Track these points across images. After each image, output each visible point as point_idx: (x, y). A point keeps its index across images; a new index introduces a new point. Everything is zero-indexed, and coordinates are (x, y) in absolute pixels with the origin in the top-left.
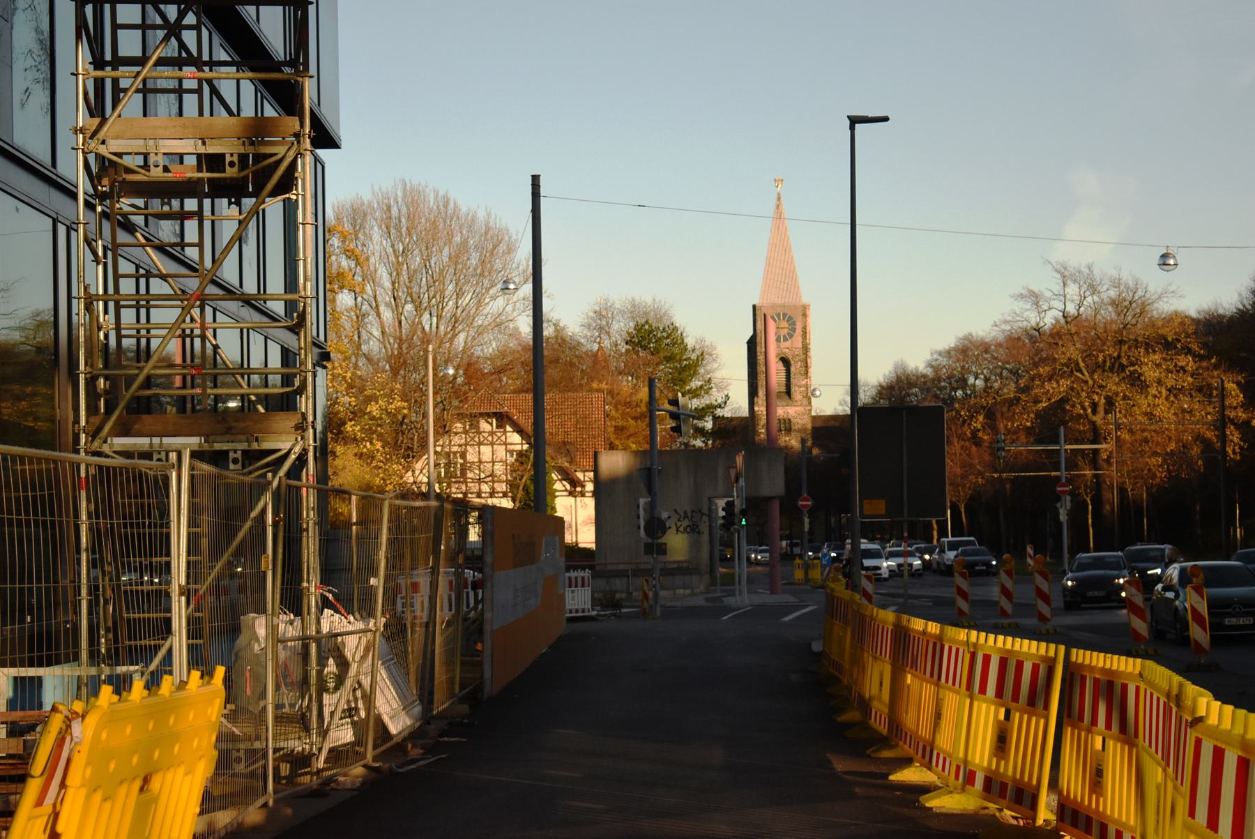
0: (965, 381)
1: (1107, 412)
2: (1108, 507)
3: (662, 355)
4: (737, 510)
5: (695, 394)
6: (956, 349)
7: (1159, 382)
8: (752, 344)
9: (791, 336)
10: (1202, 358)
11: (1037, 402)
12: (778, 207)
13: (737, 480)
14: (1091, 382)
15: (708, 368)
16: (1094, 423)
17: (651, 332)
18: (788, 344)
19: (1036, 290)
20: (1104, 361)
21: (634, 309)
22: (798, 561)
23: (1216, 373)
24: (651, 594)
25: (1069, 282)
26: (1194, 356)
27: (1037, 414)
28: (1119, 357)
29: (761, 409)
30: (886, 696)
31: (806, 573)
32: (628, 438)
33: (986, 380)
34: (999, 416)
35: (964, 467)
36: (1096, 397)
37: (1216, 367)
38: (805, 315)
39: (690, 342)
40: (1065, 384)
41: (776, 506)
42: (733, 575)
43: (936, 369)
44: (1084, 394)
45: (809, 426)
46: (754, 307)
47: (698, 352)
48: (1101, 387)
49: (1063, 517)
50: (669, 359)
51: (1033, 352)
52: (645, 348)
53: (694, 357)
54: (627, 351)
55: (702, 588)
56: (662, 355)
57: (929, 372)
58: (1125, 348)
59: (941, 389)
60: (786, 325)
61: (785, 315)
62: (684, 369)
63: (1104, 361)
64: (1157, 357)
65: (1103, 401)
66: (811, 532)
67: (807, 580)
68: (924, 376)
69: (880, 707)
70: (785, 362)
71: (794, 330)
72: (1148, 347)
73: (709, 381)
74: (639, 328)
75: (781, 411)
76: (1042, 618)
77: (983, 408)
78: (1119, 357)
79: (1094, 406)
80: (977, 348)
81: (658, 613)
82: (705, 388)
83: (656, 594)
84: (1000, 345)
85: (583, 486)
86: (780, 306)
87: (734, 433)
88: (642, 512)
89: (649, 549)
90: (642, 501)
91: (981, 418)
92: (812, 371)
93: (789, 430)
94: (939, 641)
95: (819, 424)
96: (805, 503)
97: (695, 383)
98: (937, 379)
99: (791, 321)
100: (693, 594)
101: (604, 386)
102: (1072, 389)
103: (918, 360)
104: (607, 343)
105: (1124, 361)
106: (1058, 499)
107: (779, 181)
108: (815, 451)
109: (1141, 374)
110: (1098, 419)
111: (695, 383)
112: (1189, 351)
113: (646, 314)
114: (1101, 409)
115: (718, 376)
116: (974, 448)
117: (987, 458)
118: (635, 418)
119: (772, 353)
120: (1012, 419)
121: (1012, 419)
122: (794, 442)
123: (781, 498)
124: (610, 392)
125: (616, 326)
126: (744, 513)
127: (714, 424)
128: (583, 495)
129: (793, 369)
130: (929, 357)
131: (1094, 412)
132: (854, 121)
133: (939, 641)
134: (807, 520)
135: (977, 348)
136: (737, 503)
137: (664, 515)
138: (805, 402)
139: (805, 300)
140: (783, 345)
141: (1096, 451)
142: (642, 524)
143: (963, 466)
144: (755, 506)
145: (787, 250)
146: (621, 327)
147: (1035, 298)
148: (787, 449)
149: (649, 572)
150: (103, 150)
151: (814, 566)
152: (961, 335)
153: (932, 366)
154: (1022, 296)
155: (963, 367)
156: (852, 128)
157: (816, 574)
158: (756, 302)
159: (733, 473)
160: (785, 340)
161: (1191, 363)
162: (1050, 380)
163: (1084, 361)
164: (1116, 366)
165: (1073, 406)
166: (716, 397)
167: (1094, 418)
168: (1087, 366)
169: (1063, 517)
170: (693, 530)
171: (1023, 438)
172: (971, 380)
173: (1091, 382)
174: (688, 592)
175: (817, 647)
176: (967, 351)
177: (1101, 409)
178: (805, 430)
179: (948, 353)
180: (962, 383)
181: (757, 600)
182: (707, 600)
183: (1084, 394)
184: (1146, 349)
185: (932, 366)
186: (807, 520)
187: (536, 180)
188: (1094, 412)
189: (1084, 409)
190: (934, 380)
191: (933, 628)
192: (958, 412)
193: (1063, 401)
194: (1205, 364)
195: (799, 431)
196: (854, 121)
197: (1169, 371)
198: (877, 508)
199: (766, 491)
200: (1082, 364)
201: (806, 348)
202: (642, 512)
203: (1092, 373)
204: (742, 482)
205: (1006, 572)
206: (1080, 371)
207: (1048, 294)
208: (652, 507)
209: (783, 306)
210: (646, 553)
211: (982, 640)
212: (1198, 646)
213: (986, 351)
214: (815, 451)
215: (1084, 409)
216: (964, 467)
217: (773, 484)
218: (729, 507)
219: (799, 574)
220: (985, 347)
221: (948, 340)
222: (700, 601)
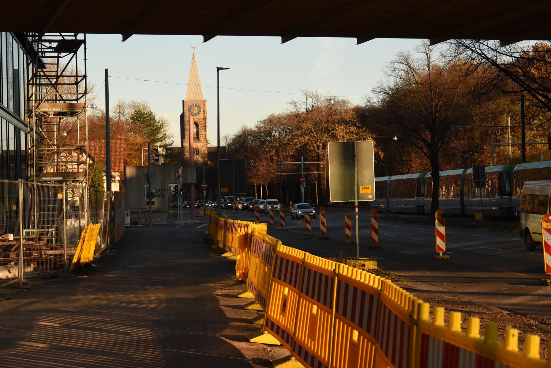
0: (271, 133)
1: (323, 149)
2: (323, 186)
3: (146, 124)
4: (179, 189)
5: (159, 140)
6: (268, 120)
7: (343, 137)
8: (182, 117)
9: (199, 113)
10: (360, 128)
11: (296, 145)
12: (193, 59)
13: (179, 178)
14: (317, 137)
15: (165, 129)
16: (318, 153)
17: (141, 114)
18: (197, 117)
19: (296, 101)
20: (322, 129)
21: (134, 106)
22: (201, 208)
23: (365, 134)
24: (149, 220)
25: (308, 98)
26: (357, 127)
27: (296, 149)
28: (328, 127)
29: (186, 144)
30: (222, 239)
31: (205, 213)
32: (132, 158)
33: (280, 133)
34: (280, 151)
35: (263, 171)
36: (318, 143)
37: (365, 131)
38: (204, 105)
39: (157, 118)
40: (307, 137)
41: (193, 187)
42: (177, 213)
43: (259, 128)
44: (314, 142)
45: (206, 151)
46: (183, 101)
47: (161, 123)
48: (321, 139)
49: (303, 190)
50: (149, 126)
51: (296, 122)
52: (138, 121)
53: (159, 125)
54: (132, 122)
55: (165, 218)
56: (146, 124)
57: (256, 129)
58: (330, 124)
59: (261, 136)
60: (197, 109)
61: (196, 105)
62: (155, 130)
63: (322, 129)
64: (342, 127)
65: (321, 144)
66: (207, 196)
67: (205, 215)
68: (254, 131)
69: (221, 243)
70: (196, 124)
71: (200, 111)
72: (339, 123)
73: (165, 134)
74: (136, 113)
75: (195, 145)
76: (282, 225)
77: (275, 147)
78: (328, 127)
79: (318, 147)
80: (276, 120)
81: (151, 226)
82: (164, 137)
83: (151, 220)
84: (285, 118)
85: (115, 178)
86: (194, 101)
87: (175, 155)
88: (145, 190)
89: (148, 203)
90: (145, 186)
91: (274, 151)
92: (208, 128)
93: (198, 153)
94: (233, 223)
95: (211, 151)
96: (204, 185)
97: (159, 136)
98: (259, 132)
99: (198, 107)
100: (162, 220)
101: (122, 137)
102: (309, 140)
103: (252, 125)
104: (122, 119)
105: (330, 129)
106: (301, 184)
107: (193, 48)
108: (209, 163)
109: (336, 134)
110: (320, 152)
111: (159, 136)
112: (354, 125)
113: (139, 106)
114: (321, 147)
115: (168, 133)
116: (270, 164)
117: (276, 167)
118: (136, 150)
119: (191, 118)
120: (285, 152)
121: (285, 152)
122: (199, 158)
123: (195, 184)
124: (125, 140)
125: (126, 112)
126: (181, 190)
127: (167, 152)
128: (115, 182)
129: (199, 127)
130: (256, 123)
131: (318, 149)
132: (219, 69)
133: (233, 223)
134: (205, 192)
135: (276, 120)
136: (179, 186)
137: (154, 191)
138: (205, 141)
139: (204, 99)
140: (195, 117)
141: (319, 164)
142: (146, 194)
143: (267, 170)
144: (186, 187)
145: (197, 77)
146: (129, 112)
147: (295, 104)
148: (196, 163)
149: (148, 212)
150: (39, 111)
151: (208, 210)
152: (269, 114)
153: (257, 127)
154: (290, 103)
155: (270, 128)
156: (218, 71)
157: (208, 212)
158: (184, 99)
159: (177, 175)
160: (196, 115)
161: (356, 130)
162: (301, 136)
163: (314, 129)
164: (327, 131)
165: (310, 147)
166: (168, 141)
167: (318, 151)
168: (316, 131)
169: (303, 190)
170: (162, 196)
171: (289, 160)
172: (274, 133)
173: (317, 137)
174: (160, 219)
175: (206, 233)
176: (272, 121)
177: (321, 147)
178: (204, 153)
179: (264, 121)
180: (270, 134)
181: (186, 222)
182: (167, 222)
183: (314, 142)
184: (338, 124)
185: (257, 127)
186: (205, 192)
187: (107, 71)
188: (318, 149)
189: (314, 147)
190: (258, 133)
191: (232, 221)
192: (265, 149)
193: (306, 144)
194: (360, 130)
195: (202, 153)
196: (219, 69)
197: (347, 133)
198: (225, 190)
199: (189, 181)
200: (313, 130)
201: (205, 119)
202: (145, 190)
203: (317, 133)
204: (181, 179)
205: (322, 214)
206: (312, 132)
207: (300, 102)
208: (149, 188)
209: (195, 101)
210: (147, 204)
211: (440, 321)
212: (323, 232)
213: (280, 121)
214: (209, 163)
215: (314, 147)
216: (263, 171)
217: (192, 179)
218: (176, 187)
219: (202, 213)
220: (279, 119)
221: (264, 116)
222: (165, 222)
